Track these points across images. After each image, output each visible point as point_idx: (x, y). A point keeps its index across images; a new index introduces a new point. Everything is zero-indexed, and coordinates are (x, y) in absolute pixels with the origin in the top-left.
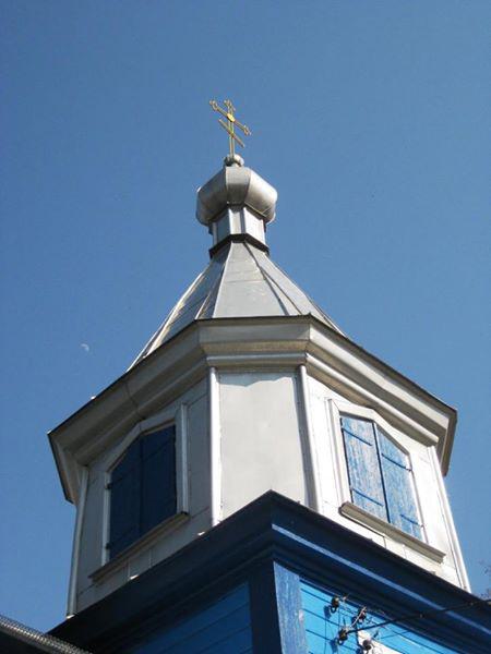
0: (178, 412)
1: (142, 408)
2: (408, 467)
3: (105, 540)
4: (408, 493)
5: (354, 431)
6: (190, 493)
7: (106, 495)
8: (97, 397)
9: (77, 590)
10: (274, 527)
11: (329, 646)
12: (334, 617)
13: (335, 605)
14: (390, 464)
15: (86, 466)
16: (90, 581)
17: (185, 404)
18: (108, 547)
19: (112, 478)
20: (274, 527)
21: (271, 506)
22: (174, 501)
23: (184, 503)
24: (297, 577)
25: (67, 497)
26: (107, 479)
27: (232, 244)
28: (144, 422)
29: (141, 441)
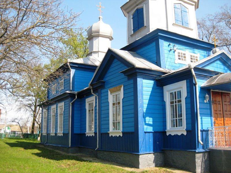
0: (143, 5)
1: (137, 3)
2: (188, 12)
3: (132, 29)
4: (187, 18)
5: (177, 7)
6: (146, 22)
7: (132, 20)
8: (63, 94)
9: (128, 37)
10: (159, 34)
11: (168, 52)
12: (170, 46)
13: (170, 44)
14: (184, 12)
15: (128, 13)
16: (130, 36)
17: (145, 4)
18: (133, 30)
19: (133, 17)
20: (159, 34)
21: (159, 30)
22: (143, 24)
23: (145, 25)
24: (163, 41)
25: (125, 16)
26: (132, 17)
27: (93, 54)
28: (137, 6)
29: (137, 10)
